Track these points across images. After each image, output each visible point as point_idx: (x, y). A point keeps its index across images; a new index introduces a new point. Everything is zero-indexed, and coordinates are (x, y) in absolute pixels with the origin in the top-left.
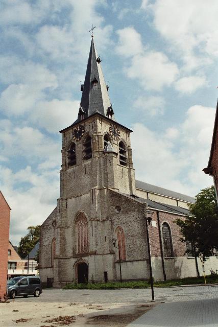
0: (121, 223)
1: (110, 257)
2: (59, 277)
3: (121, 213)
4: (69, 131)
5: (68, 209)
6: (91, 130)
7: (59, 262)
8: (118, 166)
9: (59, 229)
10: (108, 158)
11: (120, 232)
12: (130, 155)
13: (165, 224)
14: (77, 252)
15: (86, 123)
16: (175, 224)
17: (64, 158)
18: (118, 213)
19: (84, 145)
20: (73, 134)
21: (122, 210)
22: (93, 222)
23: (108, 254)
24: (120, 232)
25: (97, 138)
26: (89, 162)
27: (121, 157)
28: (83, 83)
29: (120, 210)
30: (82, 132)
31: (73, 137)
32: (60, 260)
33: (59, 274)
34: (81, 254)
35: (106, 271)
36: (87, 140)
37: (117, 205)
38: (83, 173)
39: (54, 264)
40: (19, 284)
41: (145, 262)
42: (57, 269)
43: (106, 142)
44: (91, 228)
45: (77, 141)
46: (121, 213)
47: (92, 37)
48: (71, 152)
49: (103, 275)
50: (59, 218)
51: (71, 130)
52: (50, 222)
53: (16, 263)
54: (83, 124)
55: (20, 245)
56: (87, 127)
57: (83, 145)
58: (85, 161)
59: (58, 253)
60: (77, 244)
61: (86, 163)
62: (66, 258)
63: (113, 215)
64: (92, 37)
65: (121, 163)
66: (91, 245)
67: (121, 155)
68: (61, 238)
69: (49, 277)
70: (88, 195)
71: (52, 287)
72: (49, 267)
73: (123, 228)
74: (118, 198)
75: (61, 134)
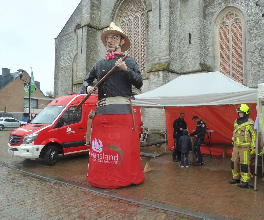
9: (85, 29)
53: (37, 100)
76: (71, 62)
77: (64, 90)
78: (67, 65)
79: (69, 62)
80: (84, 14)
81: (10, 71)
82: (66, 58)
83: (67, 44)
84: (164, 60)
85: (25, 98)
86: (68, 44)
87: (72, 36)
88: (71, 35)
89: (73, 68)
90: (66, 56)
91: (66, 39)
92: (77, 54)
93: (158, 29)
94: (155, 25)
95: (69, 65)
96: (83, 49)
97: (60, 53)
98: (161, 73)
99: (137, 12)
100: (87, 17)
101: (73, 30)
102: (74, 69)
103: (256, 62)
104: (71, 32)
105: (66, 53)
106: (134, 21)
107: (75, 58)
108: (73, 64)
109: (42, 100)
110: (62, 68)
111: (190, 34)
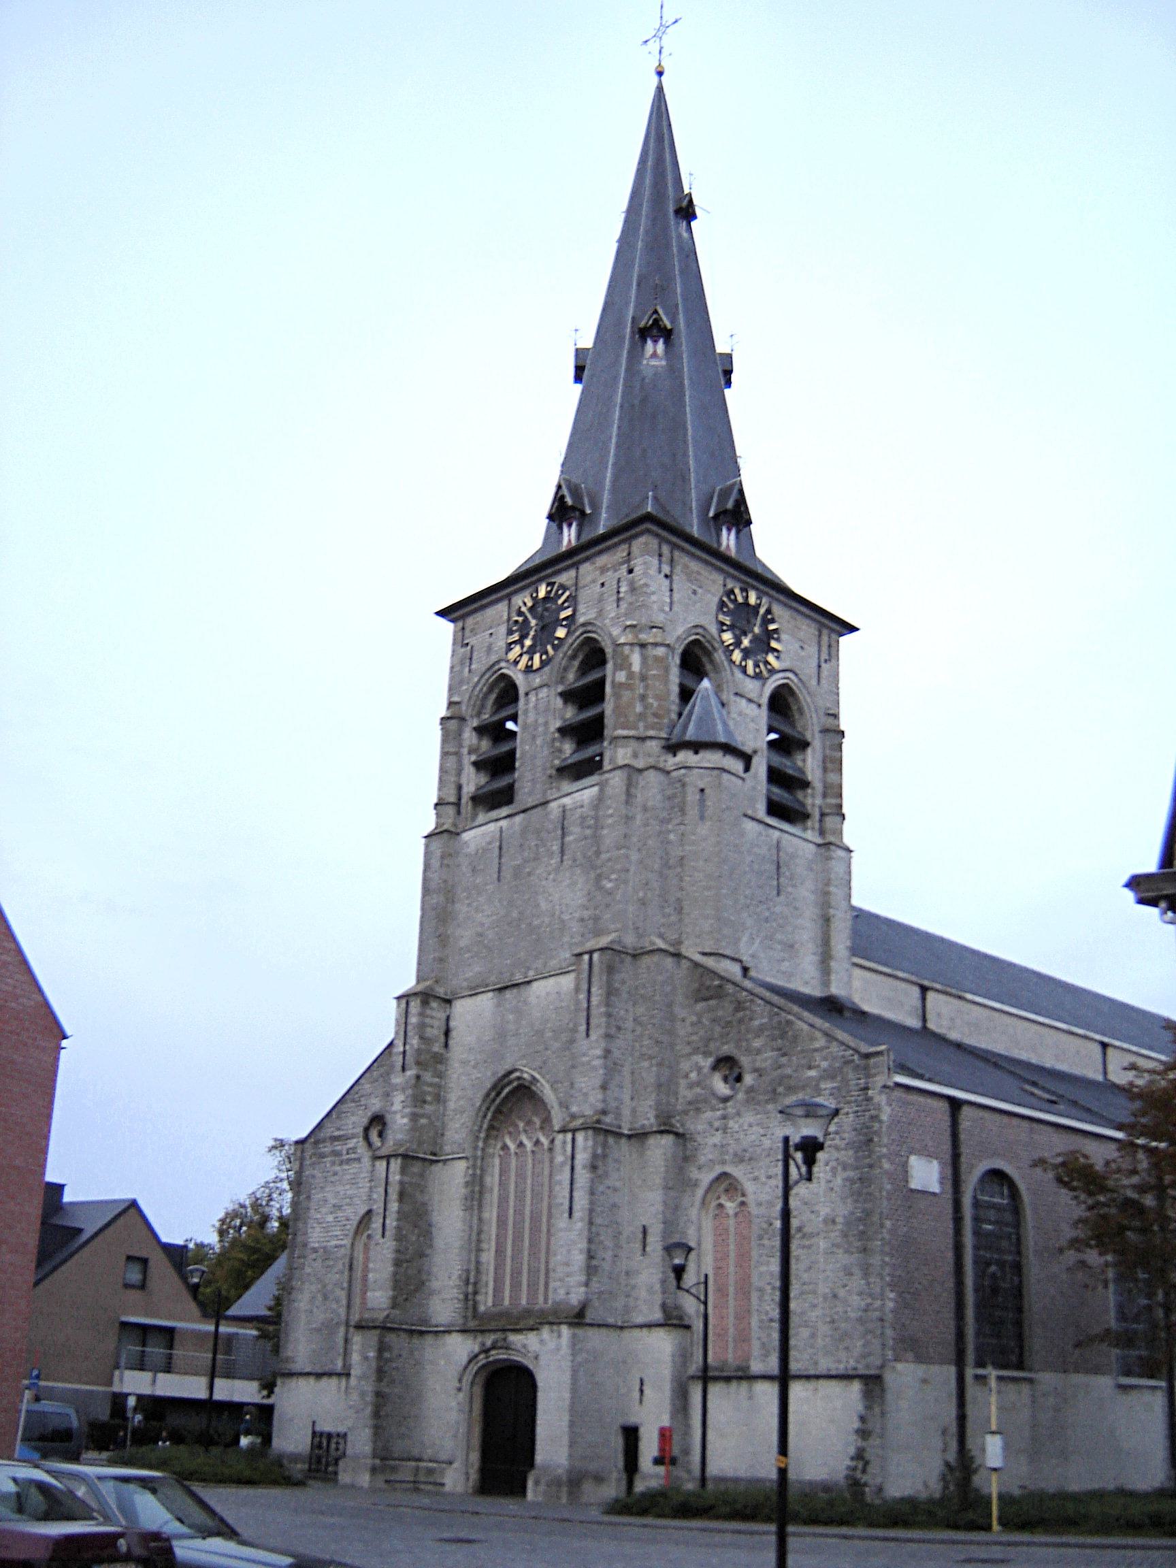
0: (739, 1159)
1: (662, 1344)
2: (377, 1430)
3: (741, 1096)
4: (491, 612)
5: (458, 1051)
6: (610, 608)
7: (382, 1348)
8: (750, 826)
9: (396, 1164)
10: (696, 780)
11: (730, 1206)
12: (833, 763)
13: (997, 1176)
14: (486, 1302)
15: (586, 568)
16: (352, 1411)
17: (452, 760)
18: (726, 1100)
19: (567, 696)
20: (510, 632)
21: (748, 1079)
22: (580, 1137)
23: (649, 1326)
24: (730, 1206)
25: (636, 659)
26: (582, 794)
27: (775, 776)
28: (587, 342)
29: (739, 1079)
30: (558, 623)
31: (509, 647)
32: (391, 1338)
33: (376, 1414)
34: (505, 1315)
35: (632, 1420)
36: (584, 669)
37: (726, 1049)
38: (551, 855)
39: (355, 1358)
40: (761, 1290)
41: (856, 1386)
42: (369, 1387)
43: (689, 683)
44: (568, 1168)
45: (529, 669)
46: (741, 1096)
47: (660, 74)
48: (496, 732)
49: (618, 1442)
50: (398, 1100)
51: (502, 607)
52: (356, 1121)
53: (170, 1331)
54: (565, 578)
55: (222, 1233)
56: (587, 596)
57: (561, 694)
58: (567, 786)
59: (379, 1298)
60: (488, 1257)
61: (566, 801)
62: (421, 1331)
63: (696, 1106)
64: (660, 74)
65: (775, 809)
66: (561, 1271)
67: (779, 761)
68: (402, 1216)
69: (326, 1427)
70: (567, 982)
71: (335, 1481)
72: (330, 1374)
73: (749, 1187)
74: (730, 1008)
75: (447, 628)
76: (346, 1235)
77: (318, 1330)
78: (334, 1243)
79: (339, 1233)
80: (395, 1112)
81: (62, 1195)
82: (330, 1218)
83: (335, 1174)
84: (575, 1298)
85: (124, 1325)
86: (340, 1173)
87: (354, 1149)
88: (351, 1143)
89: (351, 1259)
90: (331, 1213)
91: (336, 1154)
92: (369, 1212)
93: (566, 1215)
94: (562, 1204)
95: (341, 1246)
96: (388, 1222)
97: (309, 1198)
98: (565, 1330)
99: (542, 1128)
100: (405, 1125)
101: (360, 1130)
102: (355, 1262)
103: (767, 1313)
104: (353, 1136)
105: (333, 1201)
106: (533, 1152)
107: (363, 1225)
108: (353, 1244)
109: (193, 1331)
110: (315, 1250)
111: (644, 1227)
